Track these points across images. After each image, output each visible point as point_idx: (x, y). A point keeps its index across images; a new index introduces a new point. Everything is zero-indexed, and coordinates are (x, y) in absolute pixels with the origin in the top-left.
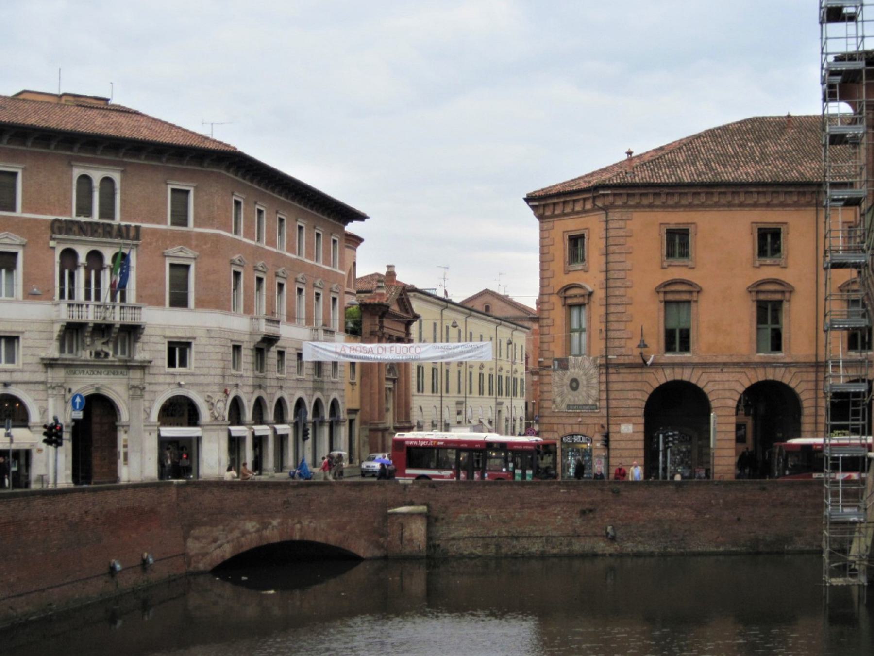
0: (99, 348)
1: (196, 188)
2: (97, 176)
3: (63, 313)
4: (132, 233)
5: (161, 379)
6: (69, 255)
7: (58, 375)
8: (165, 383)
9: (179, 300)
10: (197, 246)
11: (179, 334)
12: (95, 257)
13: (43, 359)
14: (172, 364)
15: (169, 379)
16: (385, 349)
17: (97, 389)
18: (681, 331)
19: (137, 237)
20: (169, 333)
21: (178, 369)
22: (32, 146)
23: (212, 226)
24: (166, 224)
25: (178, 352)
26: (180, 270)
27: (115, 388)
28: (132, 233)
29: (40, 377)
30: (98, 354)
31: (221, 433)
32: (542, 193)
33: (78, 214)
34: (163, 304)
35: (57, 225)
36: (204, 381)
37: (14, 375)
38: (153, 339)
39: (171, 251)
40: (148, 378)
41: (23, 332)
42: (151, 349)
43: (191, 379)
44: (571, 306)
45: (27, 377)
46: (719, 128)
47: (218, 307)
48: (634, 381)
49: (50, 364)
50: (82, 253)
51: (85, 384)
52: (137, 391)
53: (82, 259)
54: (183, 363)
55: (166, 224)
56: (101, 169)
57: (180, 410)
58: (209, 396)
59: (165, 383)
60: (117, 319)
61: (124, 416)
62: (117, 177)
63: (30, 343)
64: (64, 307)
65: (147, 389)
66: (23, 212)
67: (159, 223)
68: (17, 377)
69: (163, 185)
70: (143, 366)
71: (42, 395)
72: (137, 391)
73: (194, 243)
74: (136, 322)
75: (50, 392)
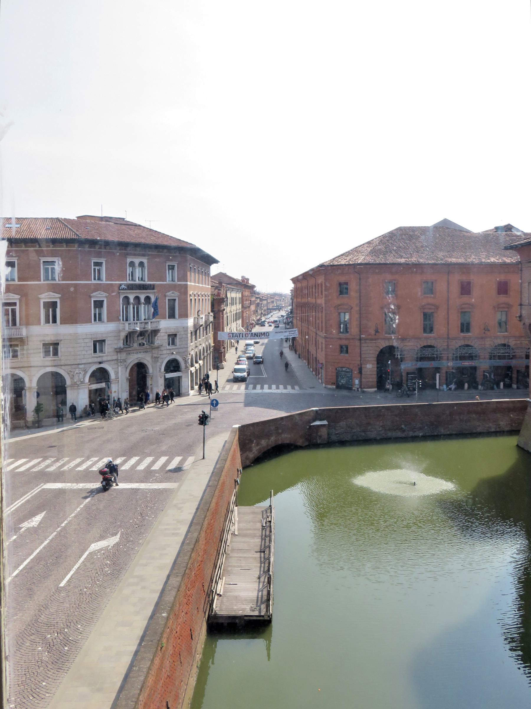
0: (140, 342)
1: (106, 261)
2: (137, 261)
3: (127, 328)
5: (165, 352)
6: (127, 299)
7: (123, 356)
12: (137, 298)
13: (116, 349)
14: (95, 351)
15: (168, 352)
17: (140, 360)
18: (49, 323)
20: (168, 331)
21: (98, 354)
24: (91, 281)
29: (115, 357)
30: (140, 344)
34: (91, 322)
39: (168, 294)
40: (160, 352)
41: (61, 340)
42: (161, 339)
45: (109, 358)
46: (395, 230)
49: (119, 351)
50: (142, 298)
51: (134, 359)
52: (156, 359)
53: (142, 300)
54: (101, 351)
55: (91, 281)
60: (150, 328)
61: (151, 370)
62: (145, 261)
63: (110, 342)
64: (127, 324)
67: (163, 281)
68: (105, 359)
71: (116, 366)
72: (156, 359)
75: (119, 364)
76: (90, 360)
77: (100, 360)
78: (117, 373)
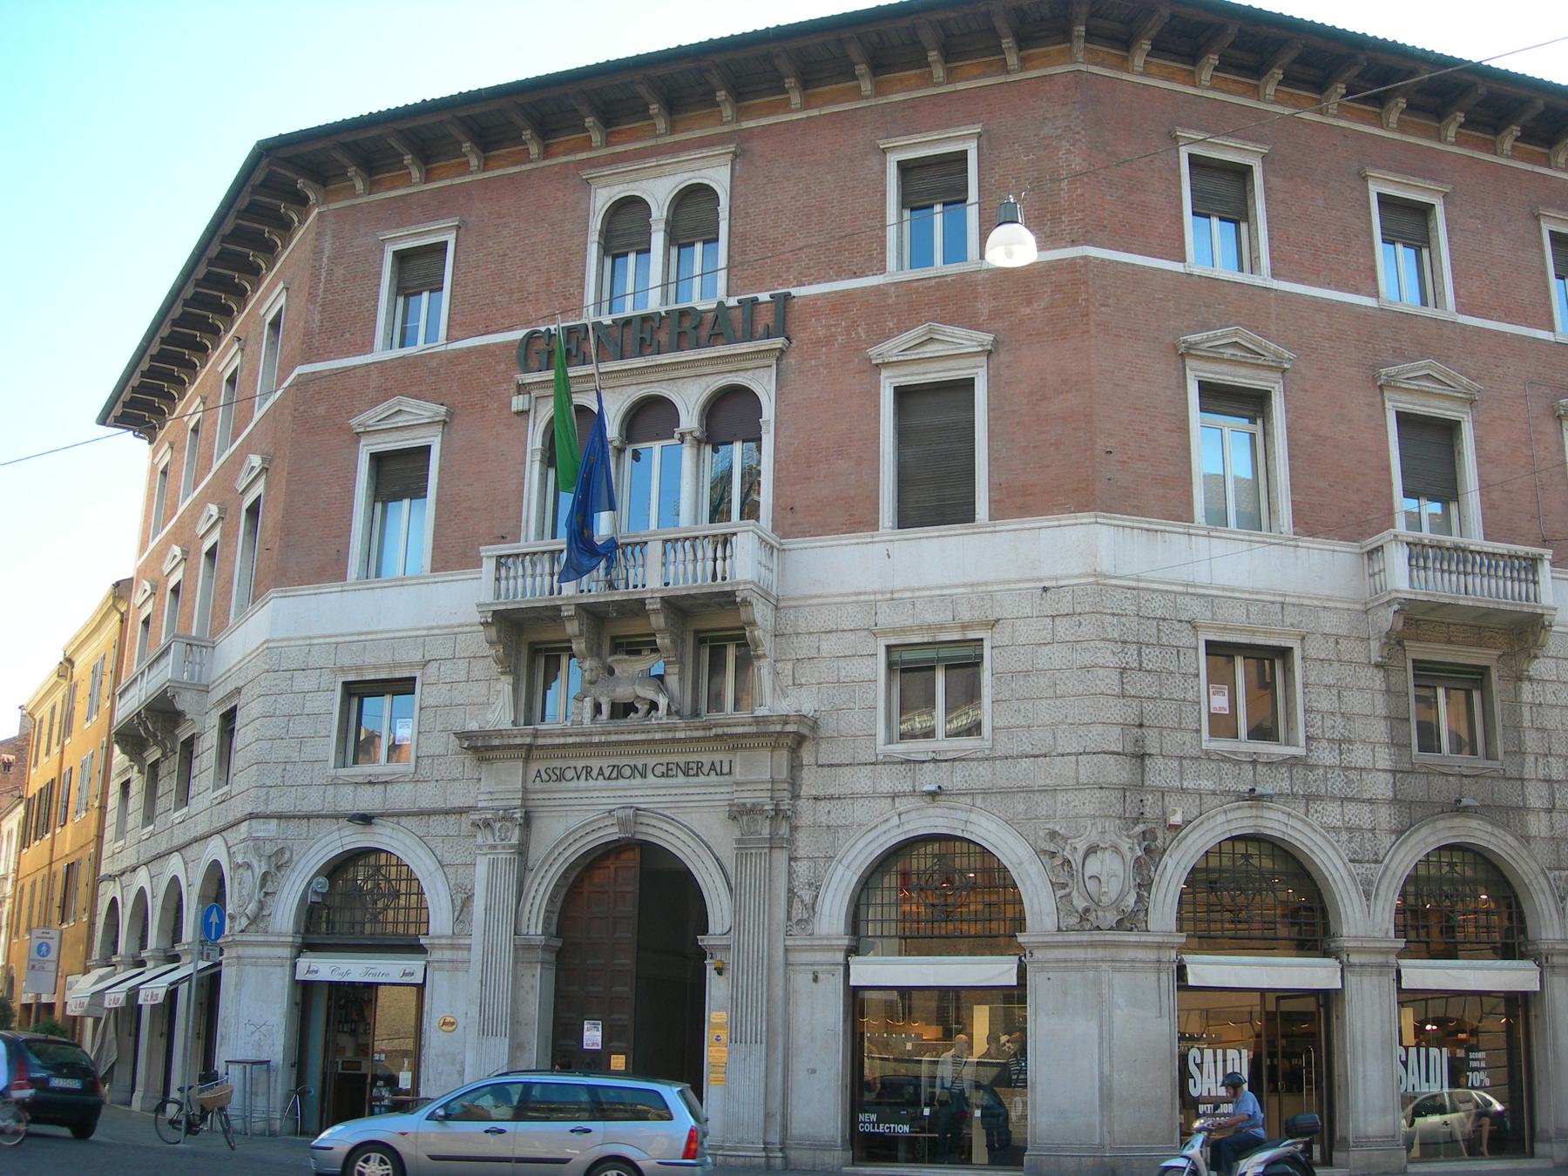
4: (765, 318)
5: (860, 780)
7: (499, 786)
8: (875, 796)
9: (936, 497)
10: (995, 315)
11: (932, 621)
15: (888, 781)
16: (348, 973)
19: (780, 327)
20: (886, 618)
22: (1343, 112)
25: (936, 671)
27: (693, 821)
28: (765, 318)
30: (623, 710)
31: (1119, 984)
34: (874, 525)
36: (1022, 788)
37: (393, 791)
39: (890, 349)
41: (238, 690)
43: (982, 774)
44: (1427, 673)
45: (428, 797)
47: (1082, 507)
52: (770, 825)
57: (937, 888)
58: (1053, 835)
59: (875, 796)
68: (402, 796)
69: (873, 161)
70: (795, 739)
73: (984, 308)
74: (479, 642)
76: (314, 801)
77: (368, 800)
78: (462, 905)
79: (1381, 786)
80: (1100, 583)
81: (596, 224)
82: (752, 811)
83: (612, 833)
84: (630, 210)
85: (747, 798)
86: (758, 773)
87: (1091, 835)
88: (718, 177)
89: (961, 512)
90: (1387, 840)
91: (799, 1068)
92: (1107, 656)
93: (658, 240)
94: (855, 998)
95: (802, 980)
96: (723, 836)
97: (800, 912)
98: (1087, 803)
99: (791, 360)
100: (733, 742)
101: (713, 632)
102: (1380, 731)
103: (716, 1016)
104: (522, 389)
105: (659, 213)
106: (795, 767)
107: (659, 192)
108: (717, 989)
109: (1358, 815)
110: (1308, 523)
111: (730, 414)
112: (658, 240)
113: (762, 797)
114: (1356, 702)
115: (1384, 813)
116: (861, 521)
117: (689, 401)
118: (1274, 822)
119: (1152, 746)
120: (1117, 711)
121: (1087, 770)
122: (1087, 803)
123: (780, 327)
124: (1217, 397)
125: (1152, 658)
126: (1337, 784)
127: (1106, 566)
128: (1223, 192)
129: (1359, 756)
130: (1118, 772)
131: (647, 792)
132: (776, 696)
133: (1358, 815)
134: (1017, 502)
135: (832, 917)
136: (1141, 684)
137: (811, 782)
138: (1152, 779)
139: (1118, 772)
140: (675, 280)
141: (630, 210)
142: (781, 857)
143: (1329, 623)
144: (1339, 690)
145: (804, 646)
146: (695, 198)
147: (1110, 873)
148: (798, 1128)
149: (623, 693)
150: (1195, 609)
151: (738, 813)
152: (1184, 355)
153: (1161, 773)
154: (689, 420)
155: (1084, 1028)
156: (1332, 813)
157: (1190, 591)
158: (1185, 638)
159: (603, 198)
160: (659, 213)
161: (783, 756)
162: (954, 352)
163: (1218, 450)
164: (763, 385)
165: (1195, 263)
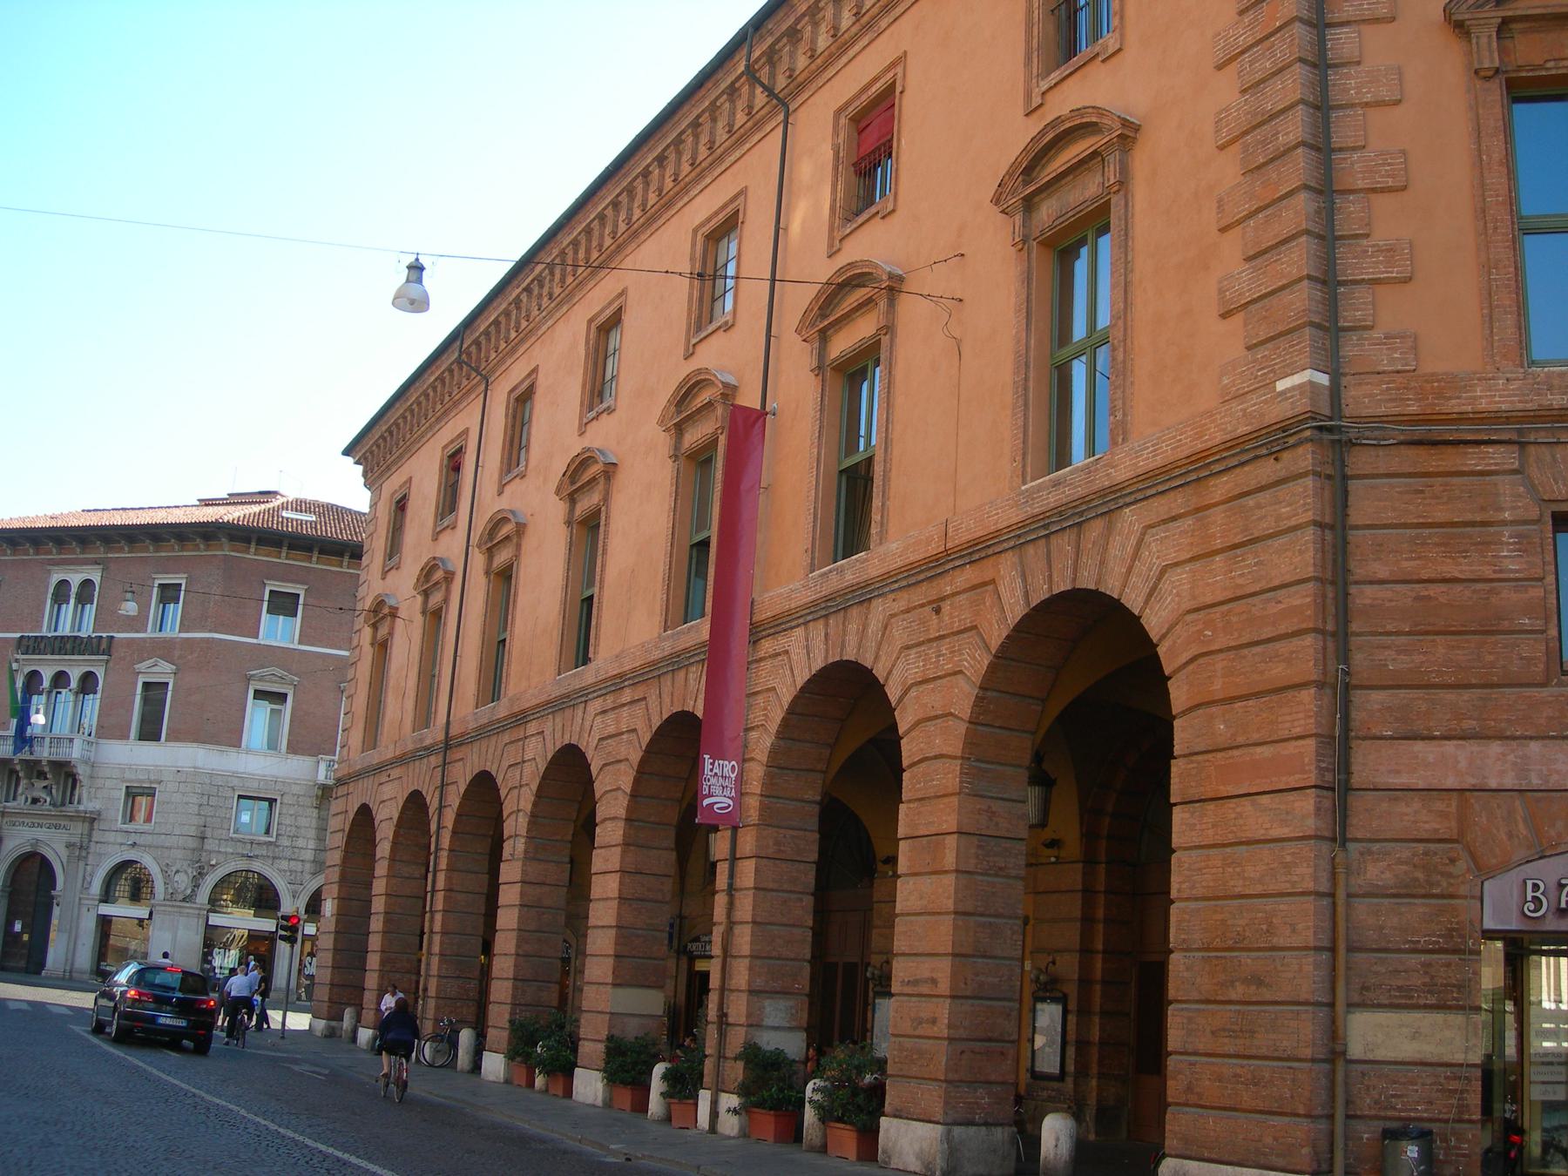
4: (104, 645)
5: (111, 837)
9: (150, 732)
11: (139, 779)
19: (108, 652)
20: (128, 775)
23: (203, 629)
26: (154, 691)
27: (55, 845)
28: (104, 645)
30: (35, 801)
32: (744, 486)
33: (300, 643)
34: (127, 738)
35: (25, 642)
38: (108, 783)
39: (142, 666)
48: (908, 611)
52: (80, 850)
56: (77, 572)
57: (129, 879)
65: (92, 850)
66: (300, 643)
70: (92, 819)
79: (309, 855)
80: (196, 772)
81: (51, 590)
82: (73, 845)
83: (28, 849)
84: (64, 584)
85: (73, 840)
86: (79, 829)
87: (178, 866)
88: (96, 577)
89: (155, 737)
90: (308, 877)
91: (80, 943)
92: (194, 799)
93: (72, 601)
94: (105, 922)
95: (84, 909)
96: (64, 853)
97: (86, 887)
98: (179, 854)
99: (111, 664)
100: (71, 818)
101: (65, 773)
102: (312, 833)
103: (55, 921)
104: (17, 661)
105: (74, 590)
106: (92, 829)
107: (75, 579)
108: (56, 911)
109: (298, 866)
110: (294, 748)
111: (88, 683)
112: (72, 601)
113: (76, 840)
114: (303, 822)
115: (308, 866)
116: (124, 736)
117: (75, 675)
118: (257, 866)
119: (208, 834)
120: (196, 820)
121: (181, 841)
122: (179, 854)
123: (108, 652)
124: (259, 695)
125: (213, 801)
126: (288, 853)
127: (200, 764)
128: (284, 604)
129: (300, 843)
130: (192, 843)
131: (41, 834)
132: (88, 802)
133: (298, 866)
134: (175, 736)
135: (96, 887)
136: (207, 811)
137: (96, 836)
138: (206, 847)
139: (192, 843)
140: (78, 622)
141: (64, 584)
142: (82, 864)
143: (296, 789)
144: (296, 816)
145: (99, 783)
146: (87, 583)
147: (183, 882)
148: (77, 965)
149: (36, 794)
150: (235, 782)
151: (69, 846)
152: (249, 679)
153: (210, 845)
154: (74, 684)
155: (168, 936)
156: (284, 865)
157: (235, 775)
158: (229, 794)
159: (56, 578)
160: (74, 590)
161: (87, 825)
162: (162, 671)
163: (258, 717)
164: (100, 673)
165: (263, 639)
